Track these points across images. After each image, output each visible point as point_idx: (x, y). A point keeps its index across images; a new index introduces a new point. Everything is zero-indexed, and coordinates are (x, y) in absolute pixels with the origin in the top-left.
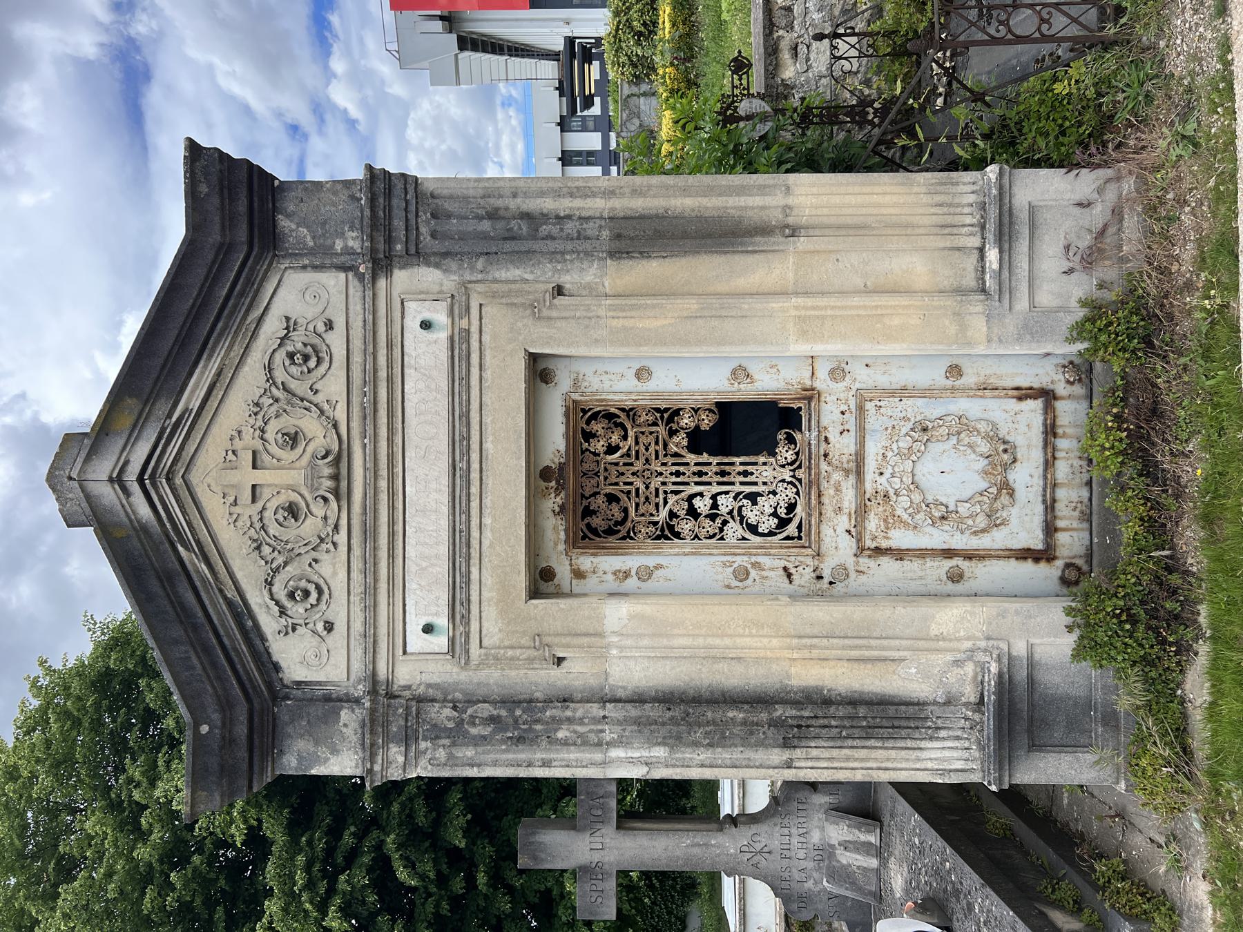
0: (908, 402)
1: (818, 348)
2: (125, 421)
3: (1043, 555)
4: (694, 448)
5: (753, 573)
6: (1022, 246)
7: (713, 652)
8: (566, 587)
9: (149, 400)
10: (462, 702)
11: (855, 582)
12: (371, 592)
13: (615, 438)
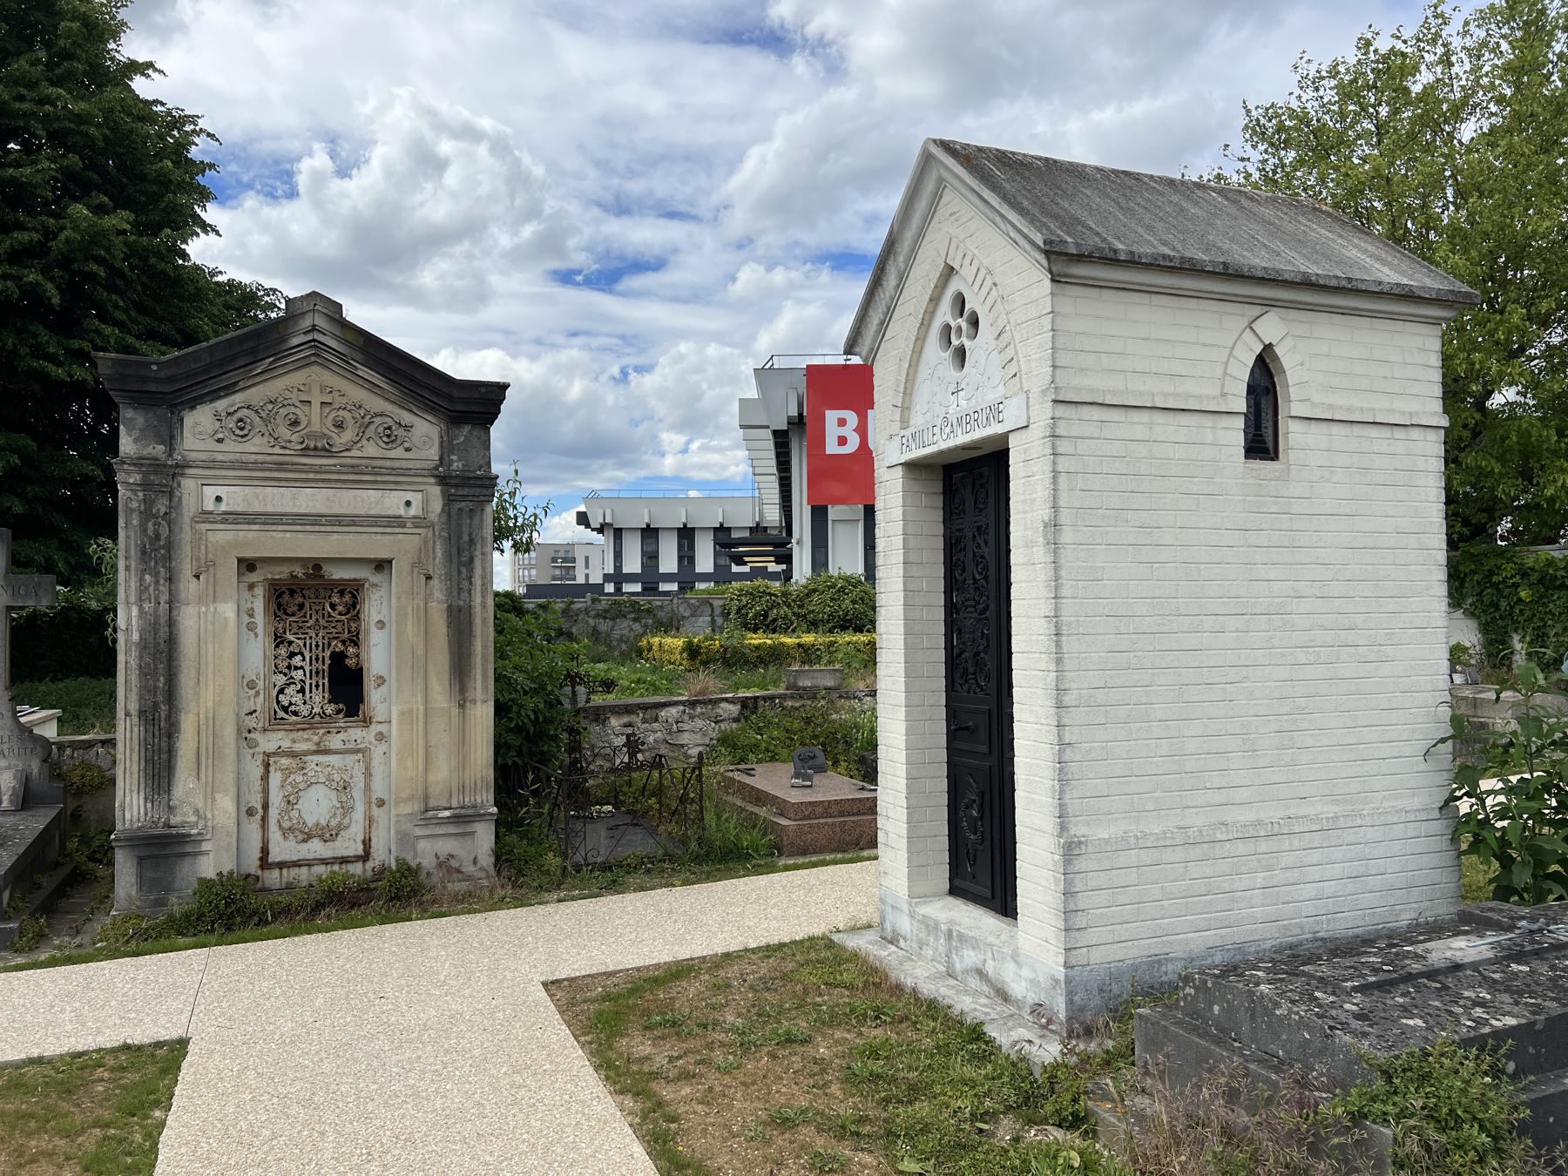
0: (362, 778)
1: (394, 722)
2: (349, 336)
3: (264, 863)
4: (334, 655)
5: (252, 692)
6: (451, 829)
7: (203, 667)
8: (245, 579)
9: (362, 350)
10: (170, 518)
11: (247, 753)
12: (244, 466)
13: (340, 608)
